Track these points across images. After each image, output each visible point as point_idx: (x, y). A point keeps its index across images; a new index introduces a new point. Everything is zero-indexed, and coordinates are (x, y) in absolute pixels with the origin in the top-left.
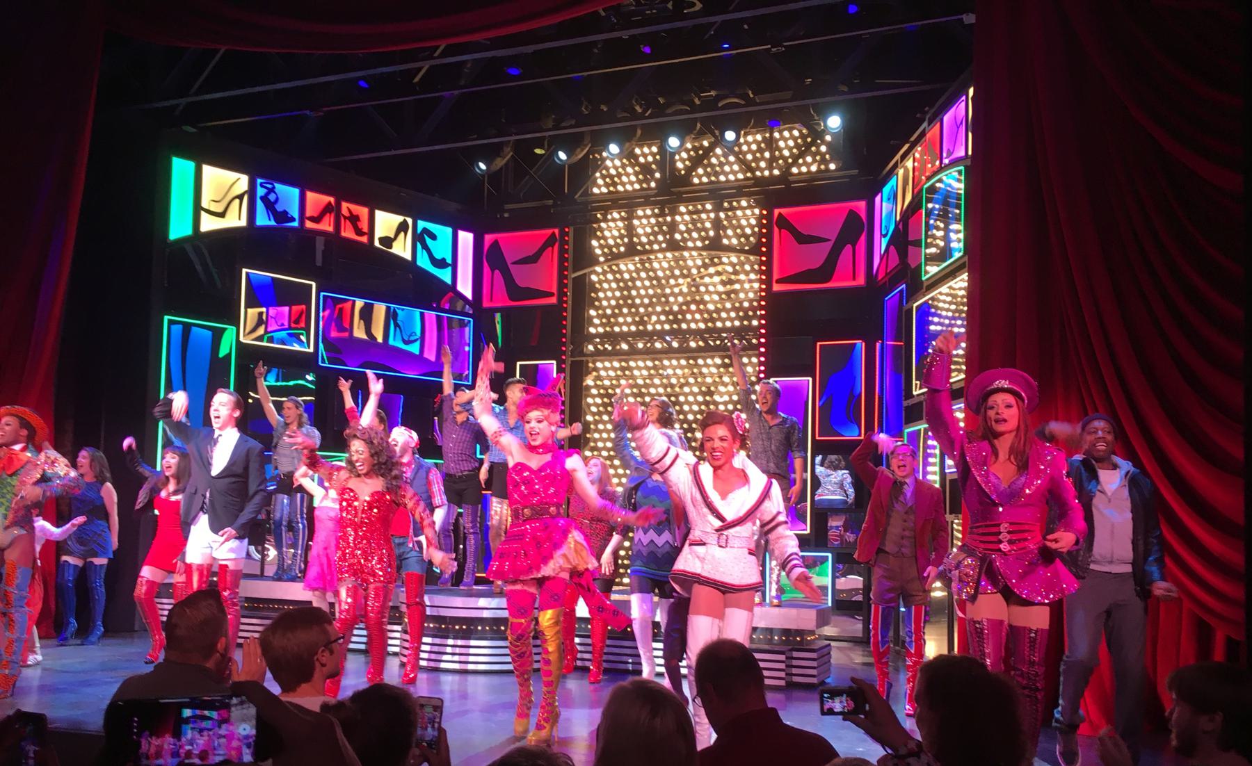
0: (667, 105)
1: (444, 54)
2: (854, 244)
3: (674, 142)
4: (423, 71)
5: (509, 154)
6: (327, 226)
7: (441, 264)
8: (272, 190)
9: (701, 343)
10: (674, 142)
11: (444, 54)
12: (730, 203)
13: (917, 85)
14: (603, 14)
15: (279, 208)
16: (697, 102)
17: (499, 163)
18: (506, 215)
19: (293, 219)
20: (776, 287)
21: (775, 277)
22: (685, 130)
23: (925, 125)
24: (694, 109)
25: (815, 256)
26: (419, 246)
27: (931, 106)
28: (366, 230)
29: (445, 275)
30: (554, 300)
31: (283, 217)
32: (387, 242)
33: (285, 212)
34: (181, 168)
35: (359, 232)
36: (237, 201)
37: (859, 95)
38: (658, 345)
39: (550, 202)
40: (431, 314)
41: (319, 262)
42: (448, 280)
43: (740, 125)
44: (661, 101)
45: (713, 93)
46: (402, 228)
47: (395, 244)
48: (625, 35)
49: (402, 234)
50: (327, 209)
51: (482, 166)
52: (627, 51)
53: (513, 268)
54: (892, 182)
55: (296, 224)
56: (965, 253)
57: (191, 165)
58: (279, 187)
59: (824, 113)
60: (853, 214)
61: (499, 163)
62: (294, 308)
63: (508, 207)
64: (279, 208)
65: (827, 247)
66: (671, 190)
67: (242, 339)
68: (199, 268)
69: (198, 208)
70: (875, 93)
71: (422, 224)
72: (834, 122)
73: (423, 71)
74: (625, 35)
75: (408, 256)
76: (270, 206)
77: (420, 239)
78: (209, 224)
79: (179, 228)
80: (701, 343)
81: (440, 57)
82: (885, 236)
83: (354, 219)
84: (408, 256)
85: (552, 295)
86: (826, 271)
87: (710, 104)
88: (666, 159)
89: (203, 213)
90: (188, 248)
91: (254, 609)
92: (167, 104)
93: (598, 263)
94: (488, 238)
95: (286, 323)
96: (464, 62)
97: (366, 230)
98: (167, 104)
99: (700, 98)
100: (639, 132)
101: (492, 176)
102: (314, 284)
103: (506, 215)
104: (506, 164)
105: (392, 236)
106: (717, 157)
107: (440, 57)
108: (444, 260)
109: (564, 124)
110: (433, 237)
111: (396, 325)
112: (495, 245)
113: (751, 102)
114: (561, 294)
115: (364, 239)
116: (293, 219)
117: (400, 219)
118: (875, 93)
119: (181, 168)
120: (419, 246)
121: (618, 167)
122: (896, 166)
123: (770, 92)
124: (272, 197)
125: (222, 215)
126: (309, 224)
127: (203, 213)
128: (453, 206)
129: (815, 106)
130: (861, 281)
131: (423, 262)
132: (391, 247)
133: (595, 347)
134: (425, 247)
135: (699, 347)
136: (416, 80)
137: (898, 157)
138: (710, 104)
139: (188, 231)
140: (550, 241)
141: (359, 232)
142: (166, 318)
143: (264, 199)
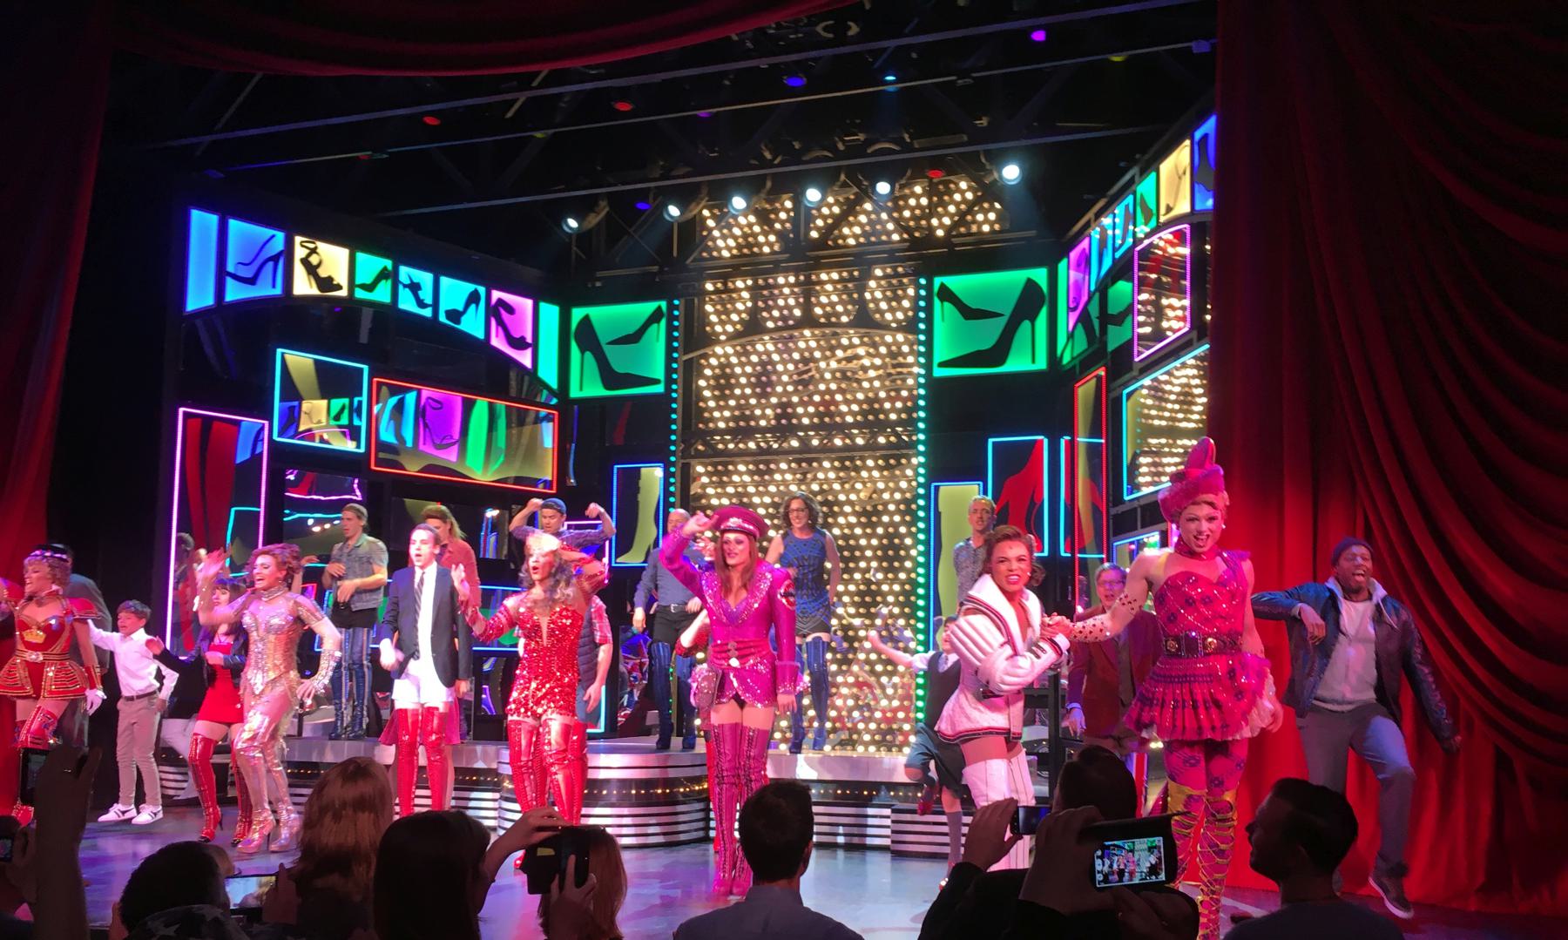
0: (806, 149)
1: (545, 84)
2: (1033, 320)
3: (813, 195)
4: (516, 106)
5: (604, 209)
6: (382, 294)
7: (519, 344)
8: (314, 251)
9: (892, 439)
10: (813, 195)
11: (545, 84)
12: (765, 280)
13: (1101, 129)
14: (735, 38)
15: (323, 273)
16: (841, 147)
17: (593, 220)
18: (598, 284)
19: (339, 287)
20: (939, 372)
21: (937, 359)
22: (827, 181)
23: (1134, 171)
24: (839, 155)
25: (986, 335)
26: (493, 323)
27: (1144, 153)
28: (429, 300)
29: (525, 358)
30: (659, 389)
31: (326, 284)
32: (455, 315)
33: (330, 279)
34: (202, 223)
35: (421, 304)
36: (270, 265)
37: (1030, 142)
38: (838, 442)
39: (655, 268)
40: (501, 405)
41: (364, 338)
42: (527, 362)
43: (893, 173)
44: (797, 145)
45: (861, 137)
46: (473, 298)
47: (464, 319)
48: (764, 63)
49: (473, 306)
50: (383, 275)
51: (573, 223)
52: (768, 83)
53: (609, 351)
54: (1085, 244)
55: (343, 293)
56: (1192, 328)
57: (213, 219)
58: (322, 247)
59: (999, 159)
60: (1031, 285)
61: (593, 220)
62: (334, 401)
63: (599, 274)
64: (323, 273)
65: (1002, 321)
66: (807, 254)
67: (275, 437)
68: (209, 351)
69: (221, 274)
70: (1062, 138)
71: (496, 295)
72: (1011, 173)
73: (516, 106)
74: (764, 63)
75: (480, 335)
76: (312, 270)
77: (496, 312)
78: (234, 292)
79: (199, 297)
80: (892, 439)
81: (540, 87)
82: (1074, 310)
83: (415, 287)
84: (479, 334)
85: (656, 382)
86: (999, 352)
87: (858, 150)
88: (803, 215)
89: (229, 281)
90: (199, 322)
91: (305, 776)
92: (184, 142)
93: (718, 342)
94: (577, 314)
95: (324, 420)
96: (560, 95)
97: (429, 300)
98: (184, 142)
99: (844, 142)
100: (769, 184)
101: (581, 235)
102: (366, 368)
103: (598, 284)
104: (599, 224)
105: (460, 308)
106: (867, 213)
107: (540, 87)
108: (523, 338)
109: (674, 173)
110: (511, 310)
111: (426, 426)
112: (586, 321)
113: (908, 148)
114: (669, 381)
115: (428, 313)
116: (339, 287)
117: (470, 287)
118: (1062, 138)
119: (202, 223)
120: (493, 323)
121: (736, 225)
122: (1088, 225)
123: (934, 136)
124: (314, 260)
125: (252, 281)
126: (360, 294)
127: (229, 281)
128: (531, 273)
129: (988, 153)
130: (1041, 364)
131: (498, 342)
132: (458, 322)
133: (758, 444)
134: (501, 323)
135: (889, 442)
136: (509, 115)
137: (1090, 215)
138: (858, 150)
139: (209, 301)
140: (655, 317)
141: (421, 304)
142: (181, 410)
143: (305, 261)
